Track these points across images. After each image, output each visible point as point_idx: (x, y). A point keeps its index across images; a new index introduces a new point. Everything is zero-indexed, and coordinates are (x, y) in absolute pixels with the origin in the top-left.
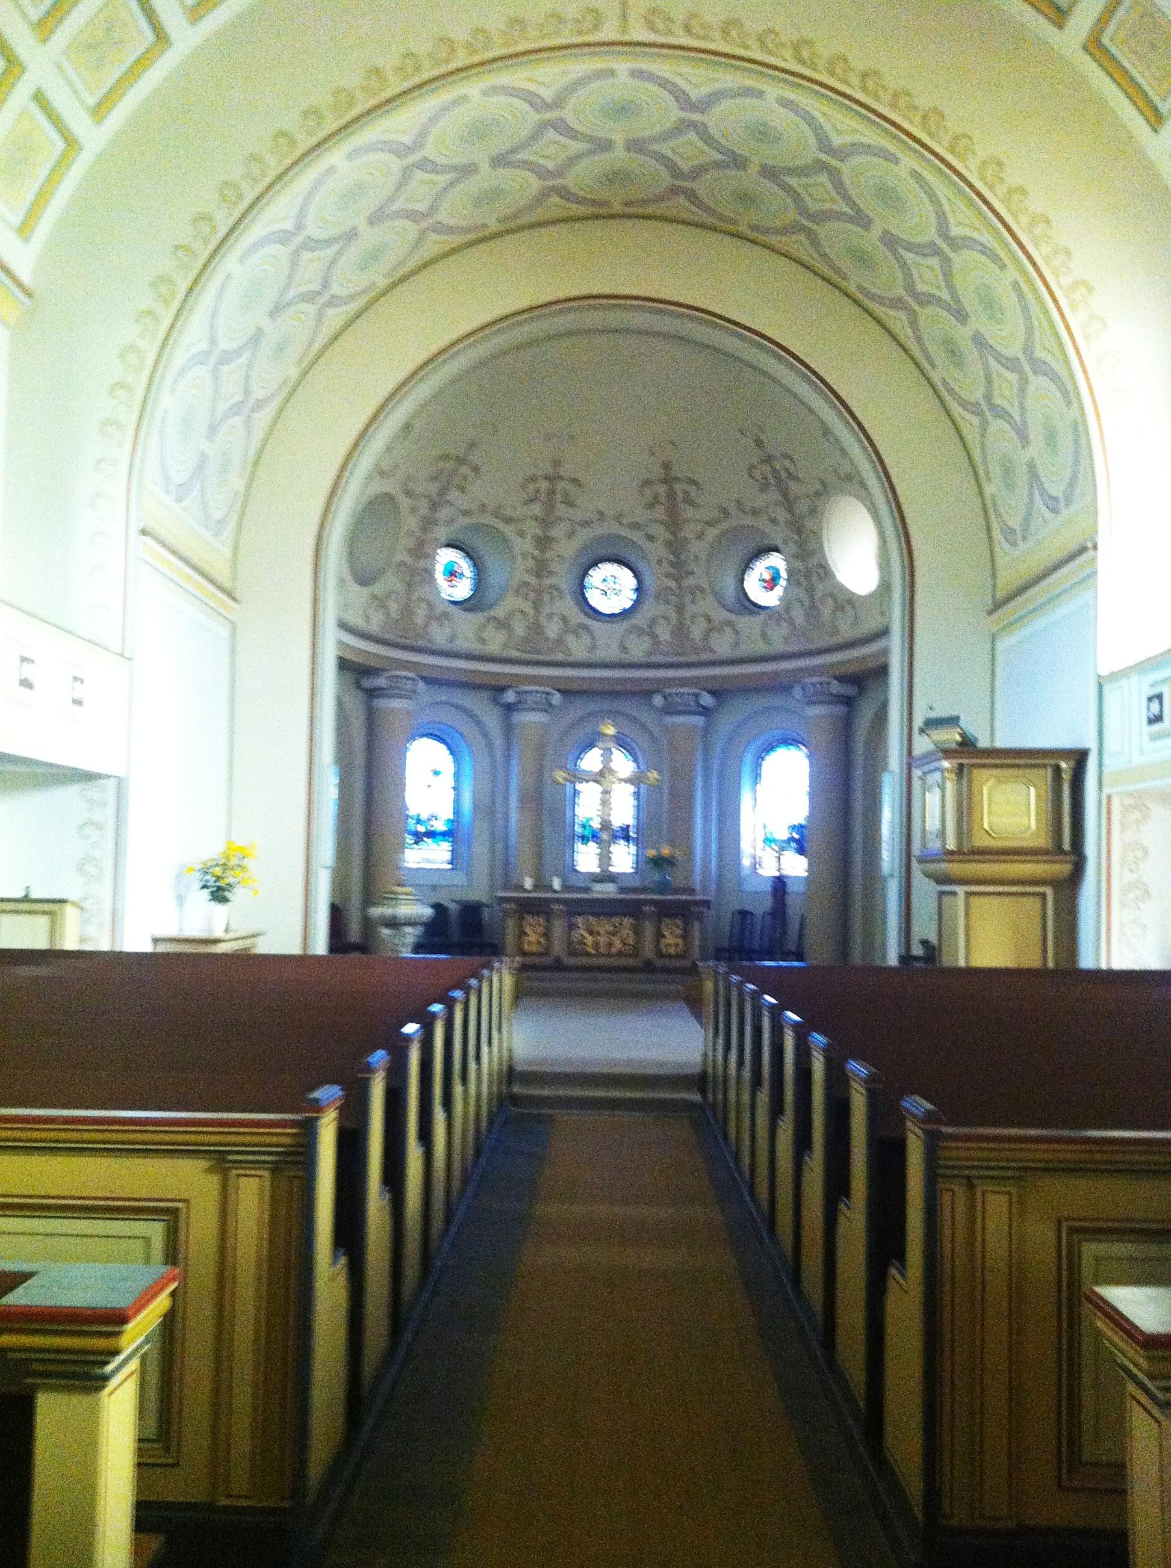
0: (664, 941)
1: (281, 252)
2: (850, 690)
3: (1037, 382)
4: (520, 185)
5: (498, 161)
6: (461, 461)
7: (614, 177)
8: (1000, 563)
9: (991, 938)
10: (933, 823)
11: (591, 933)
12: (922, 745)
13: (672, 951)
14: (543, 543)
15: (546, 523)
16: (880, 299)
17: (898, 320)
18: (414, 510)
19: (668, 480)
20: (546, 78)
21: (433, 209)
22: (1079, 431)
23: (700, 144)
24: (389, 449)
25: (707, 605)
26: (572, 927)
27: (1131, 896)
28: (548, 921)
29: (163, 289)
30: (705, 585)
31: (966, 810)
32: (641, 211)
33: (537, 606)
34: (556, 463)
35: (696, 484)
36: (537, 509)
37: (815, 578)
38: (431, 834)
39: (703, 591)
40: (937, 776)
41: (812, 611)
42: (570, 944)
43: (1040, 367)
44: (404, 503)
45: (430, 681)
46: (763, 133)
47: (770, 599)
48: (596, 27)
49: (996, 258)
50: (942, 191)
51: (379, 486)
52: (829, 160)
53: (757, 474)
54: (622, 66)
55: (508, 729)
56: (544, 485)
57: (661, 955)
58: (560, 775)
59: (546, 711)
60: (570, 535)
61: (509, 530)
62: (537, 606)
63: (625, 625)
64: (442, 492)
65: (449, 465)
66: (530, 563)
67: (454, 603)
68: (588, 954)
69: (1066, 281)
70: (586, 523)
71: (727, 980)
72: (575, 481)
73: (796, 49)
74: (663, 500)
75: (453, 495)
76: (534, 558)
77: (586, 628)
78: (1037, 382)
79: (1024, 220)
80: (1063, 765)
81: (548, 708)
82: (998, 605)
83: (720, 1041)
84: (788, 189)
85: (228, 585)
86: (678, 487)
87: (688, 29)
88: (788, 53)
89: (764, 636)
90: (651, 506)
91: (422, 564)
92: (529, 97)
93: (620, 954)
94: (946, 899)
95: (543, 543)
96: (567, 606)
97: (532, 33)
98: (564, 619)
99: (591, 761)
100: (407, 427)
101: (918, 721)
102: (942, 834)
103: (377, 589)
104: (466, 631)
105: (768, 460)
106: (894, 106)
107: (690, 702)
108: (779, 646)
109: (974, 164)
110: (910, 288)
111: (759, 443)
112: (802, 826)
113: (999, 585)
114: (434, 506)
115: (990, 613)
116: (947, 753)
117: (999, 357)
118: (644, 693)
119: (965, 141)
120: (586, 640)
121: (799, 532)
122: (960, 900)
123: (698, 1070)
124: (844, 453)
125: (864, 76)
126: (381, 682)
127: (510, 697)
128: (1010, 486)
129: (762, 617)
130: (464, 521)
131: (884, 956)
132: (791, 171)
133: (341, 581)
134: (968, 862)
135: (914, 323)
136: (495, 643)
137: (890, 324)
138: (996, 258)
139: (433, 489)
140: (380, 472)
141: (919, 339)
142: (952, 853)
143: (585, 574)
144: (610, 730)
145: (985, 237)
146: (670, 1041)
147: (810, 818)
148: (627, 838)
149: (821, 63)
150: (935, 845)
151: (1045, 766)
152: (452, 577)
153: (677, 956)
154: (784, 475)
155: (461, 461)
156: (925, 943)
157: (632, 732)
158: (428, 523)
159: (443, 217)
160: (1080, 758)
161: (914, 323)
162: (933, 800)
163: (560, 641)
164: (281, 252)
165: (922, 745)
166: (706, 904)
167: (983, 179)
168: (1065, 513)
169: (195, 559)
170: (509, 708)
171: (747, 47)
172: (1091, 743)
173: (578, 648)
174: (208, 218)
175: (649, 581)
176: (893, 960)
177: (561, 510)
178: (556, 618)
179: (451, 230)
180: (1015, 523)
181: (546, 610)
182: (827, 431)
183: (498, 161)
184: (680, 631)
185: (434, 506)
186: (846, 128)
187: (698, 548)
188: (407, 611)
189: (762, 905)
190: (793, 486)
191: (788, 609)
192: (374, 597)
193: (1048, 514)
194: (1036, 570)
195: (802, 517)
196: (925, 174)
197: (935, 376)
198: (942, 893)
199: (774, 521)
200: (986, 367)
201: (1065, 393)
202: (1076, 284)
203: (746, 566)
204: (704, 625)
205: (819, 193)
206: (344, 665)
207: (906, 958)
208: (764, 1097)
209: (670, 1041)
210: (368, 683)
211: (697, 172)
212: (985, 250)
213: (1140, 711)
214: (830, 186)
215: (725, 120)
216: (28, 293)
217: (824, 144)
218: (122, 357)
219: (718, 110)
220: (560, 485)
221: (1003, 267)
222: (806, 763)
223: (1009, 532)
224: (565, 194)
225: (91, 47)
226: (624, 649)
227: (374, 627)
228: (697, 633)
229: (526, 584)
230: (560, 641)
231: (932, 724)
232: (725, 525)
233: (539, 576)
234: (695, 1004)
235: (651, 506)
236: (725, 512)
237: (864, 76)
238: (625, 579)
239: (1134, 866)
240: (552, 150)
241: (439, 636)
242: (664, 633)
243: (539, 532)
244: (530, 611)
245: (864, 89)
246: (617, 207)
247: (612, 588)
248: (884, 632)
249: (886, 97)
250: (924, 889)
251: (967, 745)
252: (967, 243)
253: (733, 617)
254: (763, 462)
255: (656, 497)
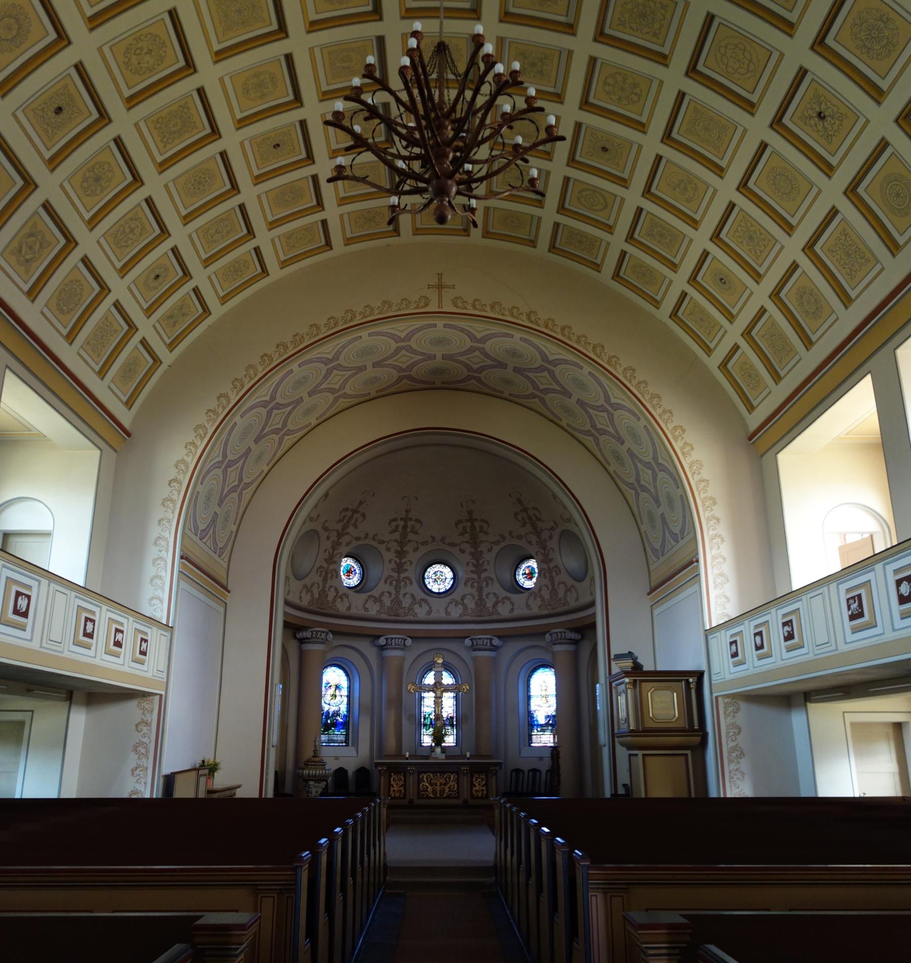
0: (475, 789)
1: (263, 411)
2: (577, 636)
3: (661, 475)
4: (387, 375)
5: (375, 365)
6: (355, 511)
7: (436, 371)
8: (652, 567)
9: (660, 781)
10: (622, 714)
11: (431, 784)
12: (615, 669)
13: (480, 794)
14: (401, 554)
15: (402, 543)
16: (580, 431)
17: (589, 441)
18: (328, 538)
19: (471, 520)
20: (401, 328)
21: (343, 387)
22: (684, 499)
23: (482, 357)
24: (316, 506)
25: (495, 588)
26: (420, 781)
27: (734, 755)
28: (405, 776)
29: (201, 432)
30: (494, 577)
31: (640, 706)
32: (452, 386)
33: (398, 589)
34: (407, 511)
35: (486, 522)
36: (397, 536)
37: (554, 573)
38: (335, 725)
39: (492, 580)
40: (622, 687)
41: (554, 592)
42: (419, 792)
43: (663, 469)
44: (324, 535)
45: (334, 633)
46: (514, 353)
47: (529, 584)
48: (426, 305)
49: (634, 414)
50: (605, 382)
51: (310, 526)
52: (548, 365)
53: (520, 517)
54: (440, 323)
55: (382, 660)
56: (401, 523)
57: (472, 796)
58: (411, 687)
59: (401, 649)
60: (416, 550)
61: (382, 548)
62: (398, 589)
63: (448, 599)
64: (344, 528)
65: (349, 514)
66: (393, 565)
67: (349, 588)
68: (431, 798)
69: (671, 426)
70: (425, 543)
71: (518, 816)
72: (418, 521)
73: (528, 316)
74: (468, 530)
75: (351, 529)
76: (395, 562)
77: (426, 601)
78: (661, 475)
79: (647, 397)
80: (691, 680)
81: (404, 647)
82: (652, 590)
83: (503, 843)
84: (529, 378)
85: (224, 582)
86: (477, 524)
87: (474, 307)
88: (524, 317)
89: (528, 605)
90: (461, 534)
91: (332, 567)
92: (393, 337)
93: (448, 797)
94: (632, 758)
95: (401, 554)
96: (415, 589)
97: (394, 308)
98: (412, 596)
99: (430, 679)
100: (326, 495)
101: (612, 657)
102: (627, 720)
103: (307, 581)
104: (357, 604)
105: (525, 510)
106: (578, 342)
107: (490, 643)
108: (535, 611)
109: (620, 370)
110: (594, 426)
111: (520, 501)
112: (554, 716)
113: (652, 579)
114: (340, 536)
115: (649, 594)
116: (627, 674)
117: (641, 462)
118: (460, 637)
119: (614, 359)
120: (425, 608)
121: (544, 548)
122: (640, 758)
123: (492, 864)
124: (565, 508)
125: (563, 329)
126: (307, 634)
127: (382, 641)
128: (654, 527)
129: (524, 596)
130: (355, 543)
131: (603, 793)
132: (530, 370)
133: (287, 578)
134: (645, 737)
135: (598, 444)
136: (373, 610)
137: (584, 441)
138: (634, 414)
139: (339, 527)
140: (310, 518)
141: (600, 451)
142: (632, 731)
143: (425, 571)
144: (440, 661)
145: (628, 404)
146: (477, 847)
147: (557, 710)
148: (452, 725)
149: (541, 322)
150: (624, 727)
151: (681, 681)
152: (349, 572)
153: (482, 798)
154: (534, 519)
155: (355, 511)
156: (625, 785)
157: (452, 660)
158: (336, 545)
159: (347, 390)
160: (699, 675)
161: (598, 444)
162: (622, 700)
163: (410, 609)
164: (263, 411)
165: (615, 669)
166: (500, 764)
167: (625, 377)
168: (682, 543)
169: (205, 567)
170: (382, 648)
171: (503, 315)
172: (704, 667)
173: (421, 612)
174: (225, 396)
175: (460, 574)
176: (608, 794)
177: (411, 536)
178: (408, 596)
179: (351, 396)
180: (657, 546)
181: (402, 592)
182: (555, 496)
183: (375, 365)
184: (480, 602)
185: (340, 536)
186: (554, 351)
187: (489, 557)
188: (323, 593)
189: (545, 766)
190: (539, 524)
191: (540, 590)
192: (305, 586)
193: (674, 543)
194: (673, 570)
195: (545, 540)
196: (597, 374)
197: (611, 469)
198: (630, 755)
199: (530, 543)
200: (636, 466)
201: (674, 480)
202: (675, 428)
203: (517, 567)
204: (494, 600)
205: (544, 380)
206: (287, 625)
207: (615, 795)
208: (545, 897)
209: (477, 847)
210: (300, 635)
211: (482, 369)
212: (630, 411)
213: (726, 651)
214: (549, 377)
215: (495, 346)
216: (129, 435)
217: (545, 358)
218: (176, 466)
219: (489, 343)
220: (410, 523)
221: (639, 419)
222: (553, 678)
223: (654, 550)
224: (411, 378)
225: (171, 317)
226: (447, 613)
227: (305, 603)
228: (489, 604)
229: (391, 576)
230: (410, 609)
231: (619, 657)
232: (502, 545)
233: (399, 573)
234: (492, 827)
235: (461, 534)
236: (503, 538)
237: (563, 329)
238: (448, 573)
239: (734, 738)
240: (404, 360)
241: (342, 607)
242: (471, 604)
243: (399, 549)
244: (393, 592)
245: (563, 335)
246: (438, 384)
247: (440, 578)
248: (592, 604)
249: (574, 338)
250: (622, 753)
251: (637, 668)
252: (618, 407)
253: (509, 595)
254: (522, 511)
255: (464, 528)
